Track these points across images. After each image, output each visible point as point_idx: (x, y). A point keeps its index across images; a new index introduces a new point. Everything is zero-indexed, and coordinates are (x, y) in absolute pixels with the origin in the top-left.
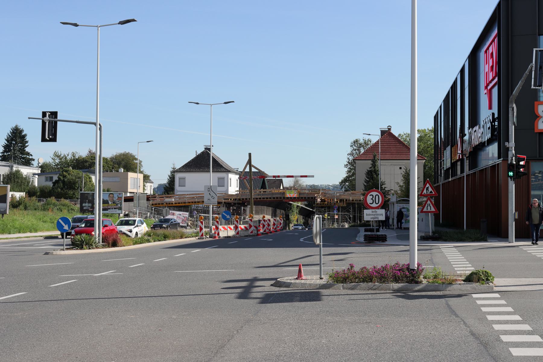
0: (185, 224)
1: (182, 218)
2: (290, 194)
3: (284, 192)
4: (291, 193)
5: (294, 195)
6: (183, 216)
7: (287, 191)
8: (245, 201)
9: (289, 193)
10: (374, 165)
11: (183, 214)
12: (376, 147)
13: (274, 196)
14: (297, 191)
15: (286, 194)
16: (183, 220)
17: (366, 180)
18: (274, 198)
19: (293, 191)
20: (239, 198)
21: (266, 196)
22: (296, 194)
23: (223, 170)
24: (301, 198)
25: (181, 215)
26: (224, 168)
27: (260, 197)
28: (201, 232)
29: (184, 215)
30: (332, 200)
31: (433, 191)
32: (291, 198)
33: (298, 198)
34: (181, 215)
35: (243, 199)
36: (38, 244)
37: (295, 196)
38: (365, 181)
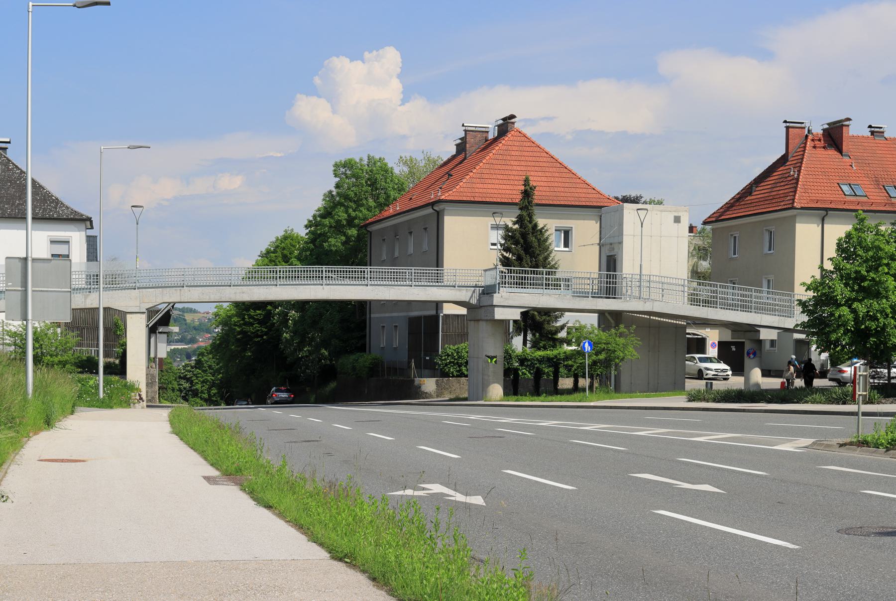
17: (504, 257)
38: (501, 260)
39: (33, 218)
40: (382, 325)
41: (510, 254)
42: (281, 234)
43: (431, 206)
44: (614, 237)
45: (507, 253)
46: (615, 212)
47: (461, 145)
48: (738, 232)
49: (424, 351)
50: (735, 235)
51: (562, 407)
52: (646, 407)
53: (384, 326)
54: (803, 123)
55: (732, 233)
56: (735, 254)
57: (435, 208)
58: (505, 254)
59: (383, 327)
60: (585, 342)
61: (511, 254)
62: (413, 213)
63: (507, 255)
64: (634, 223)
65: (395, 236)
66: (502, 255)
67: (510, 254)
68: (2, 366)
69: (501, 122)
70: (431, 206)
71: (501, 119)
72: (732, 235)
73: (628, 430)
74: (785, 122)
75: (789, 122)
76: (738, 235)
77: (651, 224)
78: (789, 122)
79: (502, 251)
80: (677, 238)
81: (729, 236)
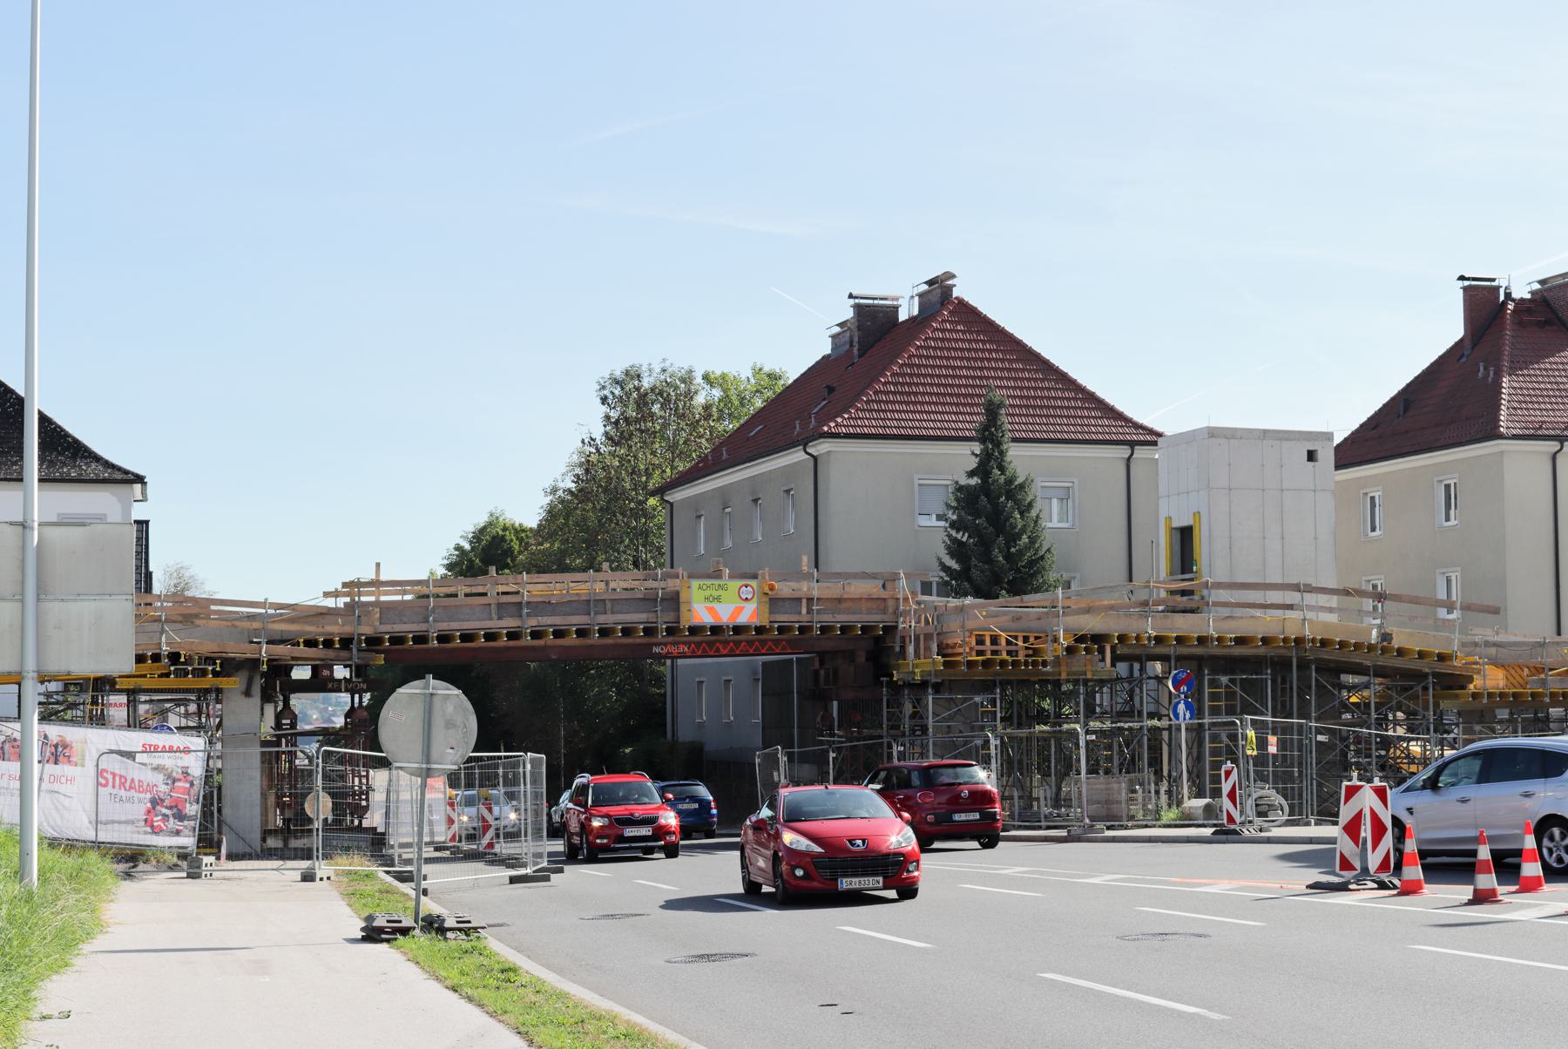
0: (178, 833)
1: (150, 788)
2: (715, 605)
3: (677, 594)
4: (718, 599)
5: (739, 610)
6: (157, 769)
7: (695, 583)
8: (410, 651)
9: (707, 599)
10: (990, 461)
11: (150, 749)
12: (891, 402)
13: (608, 619)
14: (754, 583)
15: (689, 603)
16: (156, 802)
17: (954, 540)
18: (604, 632)
19: (735, 585)
20: (367, 630)
21: (557, 620)
22: (750, 607)
23: (92, 470)
24: (781, 630)
25: (139, 757)
26: (97, 458)
27: (510, 623)
28: (1230, 779)
29: (167, 760)
30: (988, 641)
31: (1025, 634)
32: (716, 630)
33: (760, 630)
34: (130, 755)
35: (397, 640)
36: (1312, 790)
37: (743, 619)
38: (948, 548)
39: (40, 480)
40: (697, 679)
41: (964, 534)
42: (481, 520)
43: (801, 447)
44: (1188, 493)
45: (957, 532)
46: (1187, 443)
47: (840, 337)
48: (1380, 488)
49: (798, 727)
50: (1447, 482)
51: (1150, 840)
52: (1311, 838)
53: (702, 682)
54: (1494, 280)
55: (1365, 491)
56: (1373, 529)
57: (809, 450)
58: (953, 533)
59: (701, 683)
60: (1179, 702)
61: (966, 535)
62: (680, 491)
63: (959, 536)
64: (1229, 465)
65: (724, 509)
66: (949, 536)
67: (964, 534)
68: (3, 1015)
69: (925, 287)
70: (801, 447)
71: (837, 325)
72: (1366, 494)
73: (1188, 885)
74: (1462, 278)
75: (1468, 279)
76: (1379, 493)
77: (1263, 466)
78: (1468, 279)
79: (949, 529)
80: (1284, 492)
81: (1435, 483)
